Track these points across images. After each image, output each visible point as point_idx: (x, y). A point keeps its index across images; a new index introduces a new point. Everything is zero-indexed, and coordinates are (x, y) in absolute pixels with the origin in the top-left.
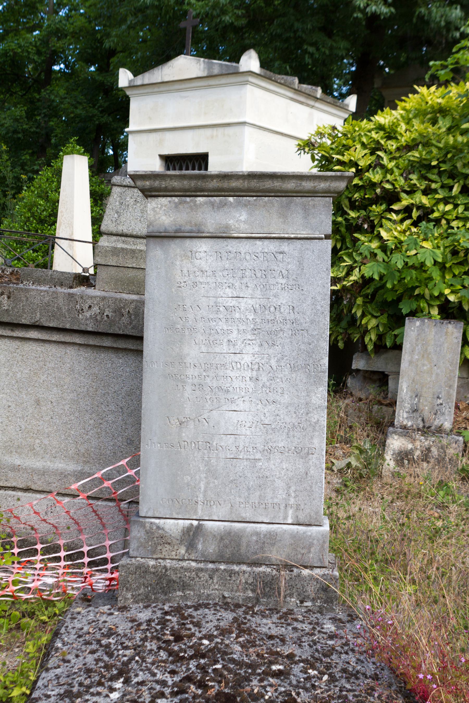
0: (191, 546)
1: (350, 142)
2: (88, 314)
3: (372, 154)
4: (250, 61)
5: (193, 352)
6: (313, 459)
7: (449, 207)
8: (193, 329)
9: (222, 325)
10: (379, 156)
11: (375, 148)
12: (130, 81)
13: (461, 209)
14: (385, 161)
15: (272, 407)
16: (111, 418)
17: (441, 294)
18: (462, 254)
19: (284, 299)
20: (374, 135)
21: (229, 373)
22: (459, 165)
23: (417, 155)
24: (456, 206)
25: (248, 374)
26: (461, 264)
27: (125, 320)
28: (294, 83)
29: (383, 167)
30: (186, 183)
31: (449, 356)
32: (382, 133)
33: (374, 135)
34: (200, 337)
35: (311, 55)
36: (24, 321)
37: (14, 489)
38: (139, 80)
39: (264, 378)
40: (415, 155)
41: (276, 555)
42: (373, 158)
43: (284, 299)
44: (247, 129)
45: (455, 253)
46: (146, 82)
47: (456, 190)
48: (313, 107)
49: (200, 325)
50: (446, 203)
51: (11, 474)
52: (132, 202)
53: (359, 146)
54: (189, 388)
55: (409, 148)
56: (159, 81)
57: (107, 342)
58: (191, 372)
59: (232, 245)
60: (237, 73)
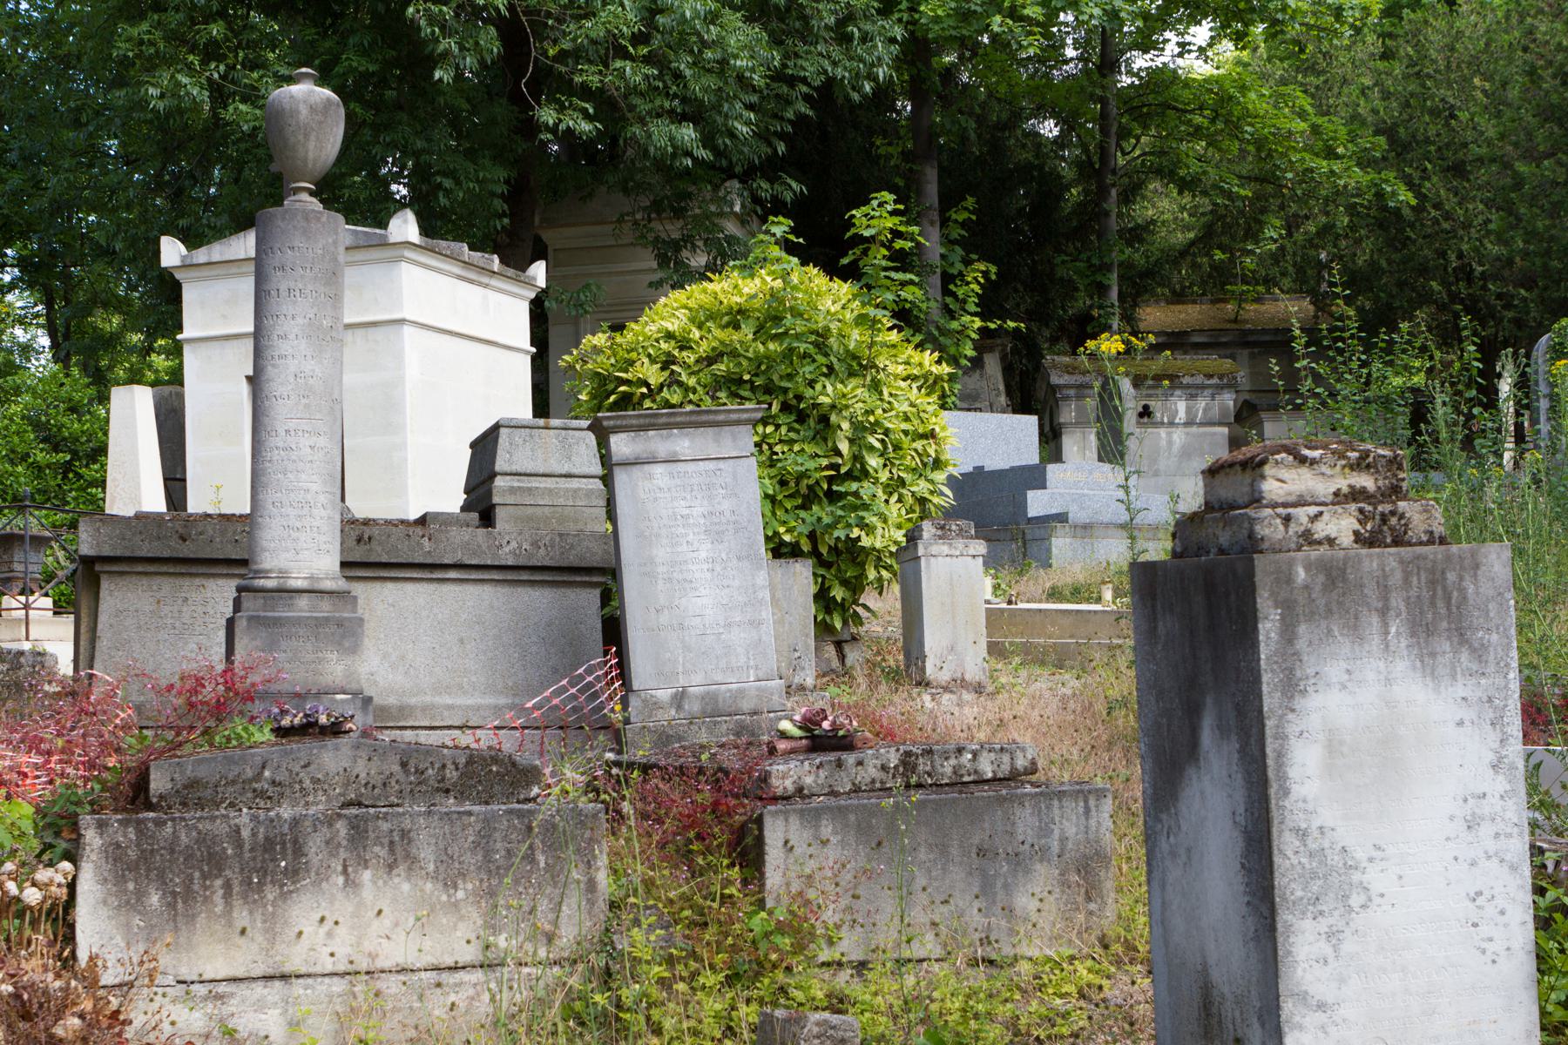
0: (679, 707)
1: (634, 355)
2: (507, 549)
3: (663, 369)
4: (405, 227)
5: (661, 553)
6: (764, 627)
7: (770, 429)
8: (658, 536)
9: (681, 530)
10: (673, 372)
11: (667, 362)
12: (183, 258)
13: (784, 430)
14: (684, 378)
15: (727, 591)
16: (534, 649)
17: (776, 533)
18: (792, 484)
19: (726, 505)
20: (664, 346)
21: (693, 568)
22: (775, 378)
23: (723, 367)
24: (778, 427)
25: (706, 566)
26: (790, 496)
27: (542, 551)
28: (462, 253)
29: (680, 384)
30: (642, 421)
31: (800, 600)
32: (673, 342)
33: (664, 346)
34: (665, 541)
35: (447, 192)
36: (446, 561)
37: (449, 727)
38: (201, 255)
39: (718, 568)
40: (721, 367)
41: (746, 706)
42: (666, 373)
43: (726, 505)
44: (407, 329)
45: (783, 483)
46: (216, 257)
47: (775, 408)
48: (486, 286)
49: (664, 532)
50: (765, 425)
51: (446, 713)
52: (521, 441)
53: (646, 360)
54: (660, 582)
55: (710, 360)
56: (242, 256)
57: (525, 576)
58: (661, 569)
59: (680, 467)
60: (384, 244)
